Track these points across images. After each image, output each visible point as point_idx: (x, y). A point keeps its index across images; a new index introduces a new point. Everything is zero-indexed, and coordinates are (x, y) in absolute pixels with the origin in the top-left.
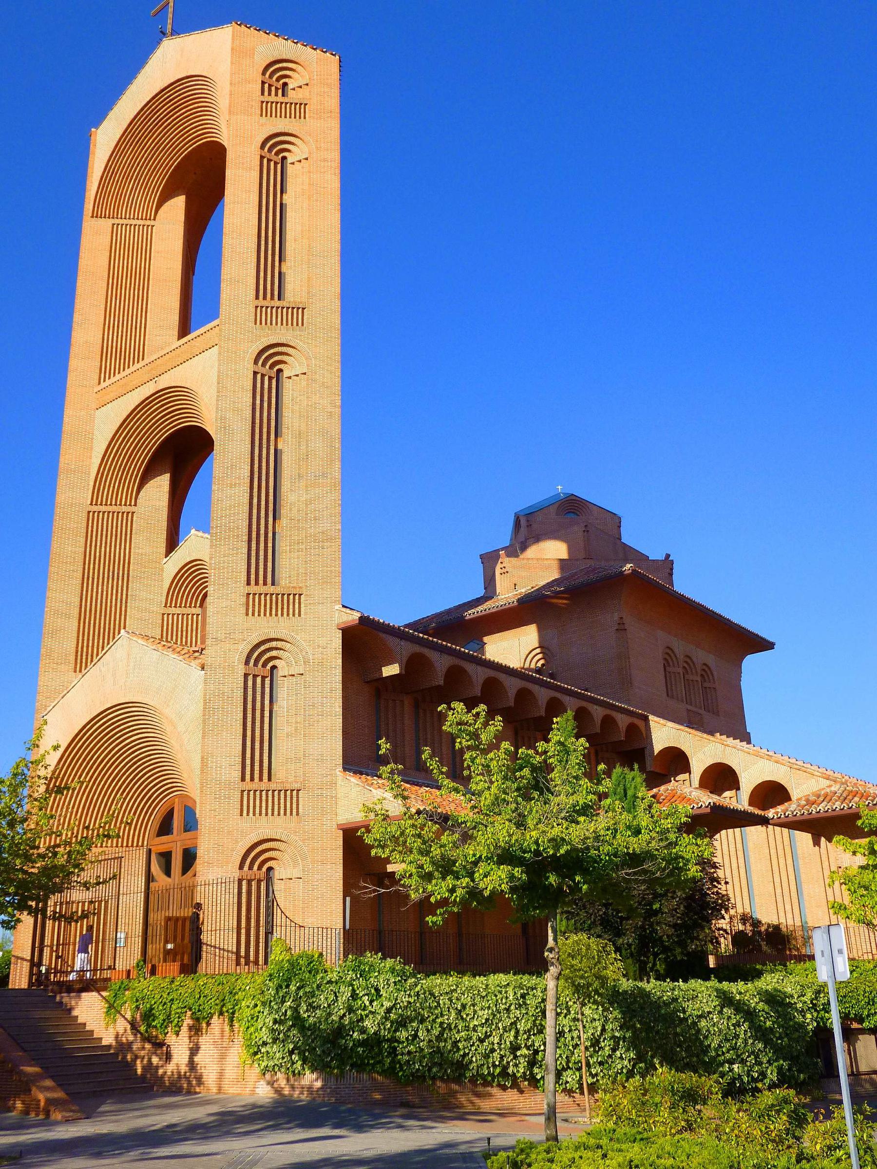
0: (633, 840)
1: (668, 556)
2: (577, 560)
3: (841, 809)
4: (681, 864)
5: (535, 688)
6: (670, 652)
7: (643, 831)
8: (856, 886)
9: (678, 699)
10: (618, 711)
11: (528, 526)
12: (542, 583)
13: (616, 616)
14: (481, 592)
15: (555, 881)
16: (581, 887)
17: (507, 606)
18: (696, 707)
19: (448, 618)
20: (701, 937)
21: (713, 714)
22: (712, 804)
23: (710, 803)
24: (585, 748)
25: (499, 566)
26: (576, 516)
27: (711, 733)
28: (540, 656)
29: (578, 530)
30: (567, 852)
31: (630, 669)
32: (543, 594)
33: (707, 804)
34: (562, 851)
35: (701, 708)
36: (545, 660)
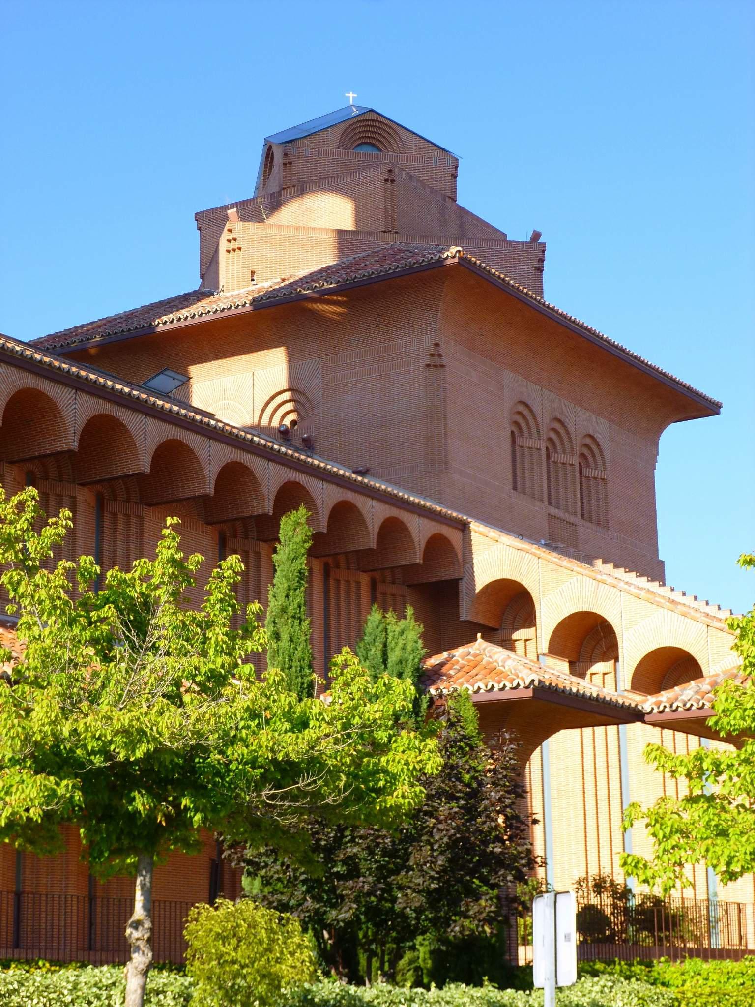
0: (289, 737)
1: (536, 236)
2: (369, 233)
3: (487, 691)
4: (381, 784)
5: (257, 465)
6: (526, 412)
7: (311, 724)
8: (668, 830)
9: (533, 496)
10: (412, 512)
11: (285, 164)
12: (303, 272)
13: (427, 342)
14: (194, 284)
15: (143, 805)
16: (191, 818)
17: (233, 311)
18: (567, 511)
19: (125, 328)
20: (471, 913)
21: (599, 524)
22: (536, 683)
23: (533, 681)
24: (237, 573)
25: (225, 236)
26: (375, 152)
27: (588, 559)
28: (290, 406)
29: (375, 176)
30: (148, 755)
31: (446, 438)
32: (299, 293)
33: (527, 683)
34: (139, 754)
35: (575, 514)
36: (299, 414)
